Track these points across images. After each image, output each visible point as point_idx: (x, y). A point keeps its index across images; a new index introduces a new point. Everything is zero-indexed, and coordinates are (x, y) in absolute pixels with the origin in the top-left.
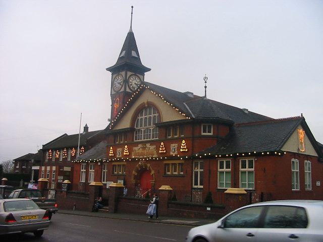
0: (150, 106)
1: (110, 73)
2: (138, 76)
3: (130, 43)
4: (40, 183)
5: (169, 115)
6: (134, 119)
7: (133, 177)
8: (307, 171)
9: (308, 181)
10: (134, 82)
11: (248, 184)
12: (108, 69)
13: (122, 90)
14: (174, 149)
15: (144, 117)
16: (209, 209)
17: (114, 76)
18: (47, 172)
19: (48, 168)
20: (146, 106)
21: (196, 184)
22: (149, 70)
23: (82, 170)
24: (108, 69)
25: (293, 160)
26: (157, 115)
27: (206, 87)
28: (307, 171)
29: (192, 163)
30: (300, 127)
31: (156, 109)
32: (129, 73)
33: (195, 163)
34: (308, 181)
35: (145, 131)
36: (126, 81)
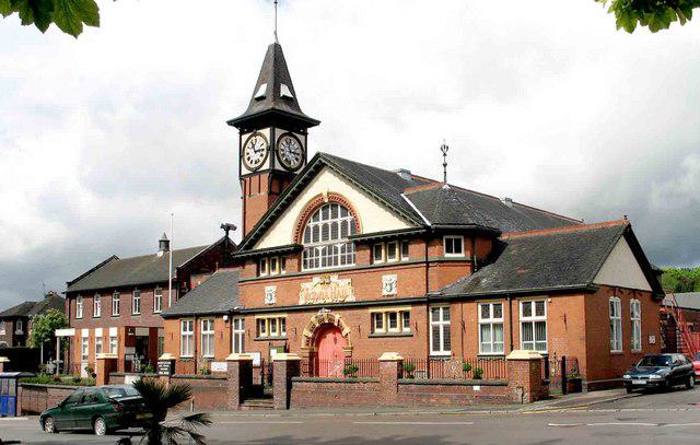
0: (334, 204)
1: (236, 131)
2: (295, 137)
3: (277, 67)
4: (525, 370)
5: (376, 219)
6: (301, 228)
7: (304, 340)
8: (637, 318)
9: (637, 341)
10: (288, 149)
11: (494, 345)
12: (230, 123)
13: (266, 166)
14: (391, 285)
15: (321, 223)
16: (476, 388)
17: (245, 137)
18: (95, 341)
19: (99, 332)
20: (326, 201)
21: (436, 348)
22: (314, 123)
23: (183, 333)
24: (230, 123)
25: (612, 299)
26: (349, 219)
27: (445, 165)
28: (637, 318)
29: (428, 311)
30: (623, 240)
31: (346, 209)
32: (279, 132)
33: (434, 310)
34: (637, 341)
35: (324, 251)
36: (273, 150)
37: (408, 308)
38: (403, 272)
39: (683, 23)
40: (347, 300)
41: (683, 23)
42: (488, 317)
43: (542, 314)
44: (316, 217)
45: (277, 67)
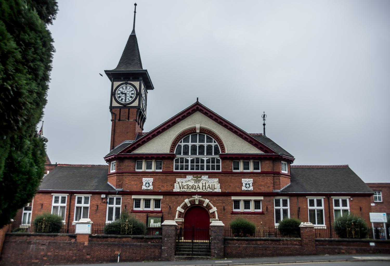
3: (132, 48)
15: (190, 144)
37: (161, 197)
38: (256, 178)
39: (51, 34)
40: (216, 191)
41: (51, 34)
42: (313, 205)
43: (346, 206)
44: (186, 140)
45: (132, 48)
